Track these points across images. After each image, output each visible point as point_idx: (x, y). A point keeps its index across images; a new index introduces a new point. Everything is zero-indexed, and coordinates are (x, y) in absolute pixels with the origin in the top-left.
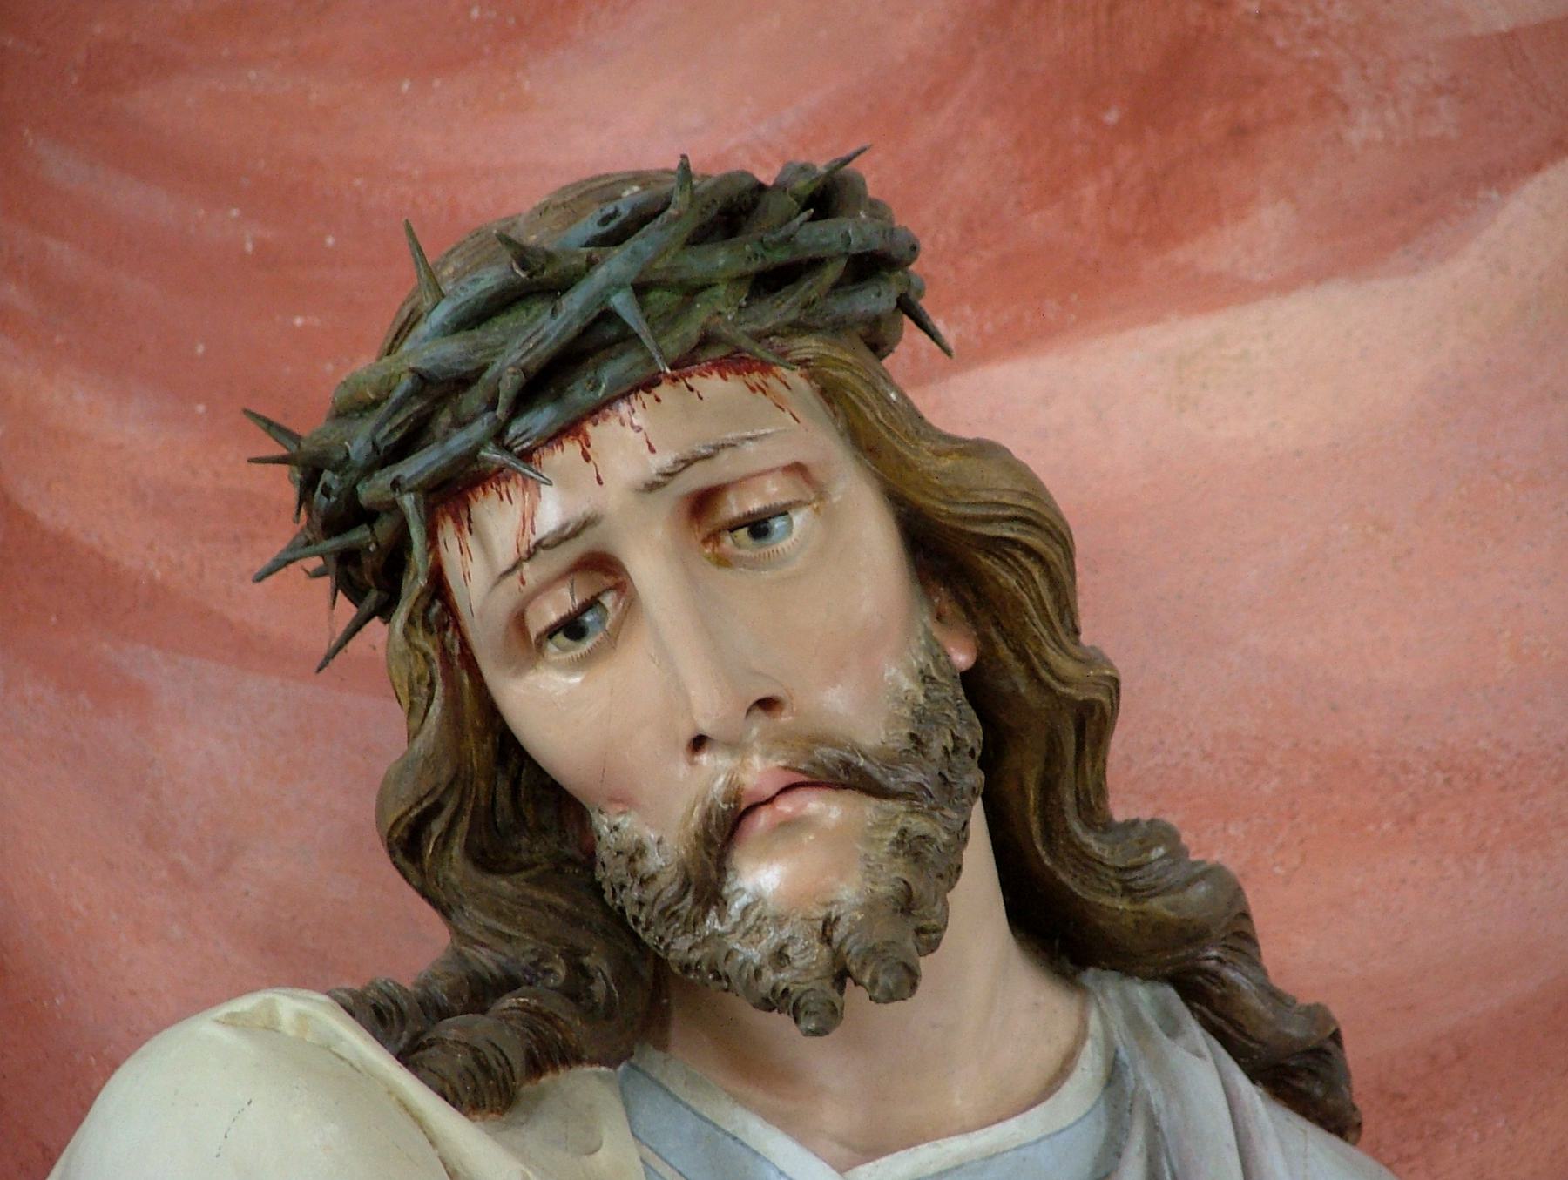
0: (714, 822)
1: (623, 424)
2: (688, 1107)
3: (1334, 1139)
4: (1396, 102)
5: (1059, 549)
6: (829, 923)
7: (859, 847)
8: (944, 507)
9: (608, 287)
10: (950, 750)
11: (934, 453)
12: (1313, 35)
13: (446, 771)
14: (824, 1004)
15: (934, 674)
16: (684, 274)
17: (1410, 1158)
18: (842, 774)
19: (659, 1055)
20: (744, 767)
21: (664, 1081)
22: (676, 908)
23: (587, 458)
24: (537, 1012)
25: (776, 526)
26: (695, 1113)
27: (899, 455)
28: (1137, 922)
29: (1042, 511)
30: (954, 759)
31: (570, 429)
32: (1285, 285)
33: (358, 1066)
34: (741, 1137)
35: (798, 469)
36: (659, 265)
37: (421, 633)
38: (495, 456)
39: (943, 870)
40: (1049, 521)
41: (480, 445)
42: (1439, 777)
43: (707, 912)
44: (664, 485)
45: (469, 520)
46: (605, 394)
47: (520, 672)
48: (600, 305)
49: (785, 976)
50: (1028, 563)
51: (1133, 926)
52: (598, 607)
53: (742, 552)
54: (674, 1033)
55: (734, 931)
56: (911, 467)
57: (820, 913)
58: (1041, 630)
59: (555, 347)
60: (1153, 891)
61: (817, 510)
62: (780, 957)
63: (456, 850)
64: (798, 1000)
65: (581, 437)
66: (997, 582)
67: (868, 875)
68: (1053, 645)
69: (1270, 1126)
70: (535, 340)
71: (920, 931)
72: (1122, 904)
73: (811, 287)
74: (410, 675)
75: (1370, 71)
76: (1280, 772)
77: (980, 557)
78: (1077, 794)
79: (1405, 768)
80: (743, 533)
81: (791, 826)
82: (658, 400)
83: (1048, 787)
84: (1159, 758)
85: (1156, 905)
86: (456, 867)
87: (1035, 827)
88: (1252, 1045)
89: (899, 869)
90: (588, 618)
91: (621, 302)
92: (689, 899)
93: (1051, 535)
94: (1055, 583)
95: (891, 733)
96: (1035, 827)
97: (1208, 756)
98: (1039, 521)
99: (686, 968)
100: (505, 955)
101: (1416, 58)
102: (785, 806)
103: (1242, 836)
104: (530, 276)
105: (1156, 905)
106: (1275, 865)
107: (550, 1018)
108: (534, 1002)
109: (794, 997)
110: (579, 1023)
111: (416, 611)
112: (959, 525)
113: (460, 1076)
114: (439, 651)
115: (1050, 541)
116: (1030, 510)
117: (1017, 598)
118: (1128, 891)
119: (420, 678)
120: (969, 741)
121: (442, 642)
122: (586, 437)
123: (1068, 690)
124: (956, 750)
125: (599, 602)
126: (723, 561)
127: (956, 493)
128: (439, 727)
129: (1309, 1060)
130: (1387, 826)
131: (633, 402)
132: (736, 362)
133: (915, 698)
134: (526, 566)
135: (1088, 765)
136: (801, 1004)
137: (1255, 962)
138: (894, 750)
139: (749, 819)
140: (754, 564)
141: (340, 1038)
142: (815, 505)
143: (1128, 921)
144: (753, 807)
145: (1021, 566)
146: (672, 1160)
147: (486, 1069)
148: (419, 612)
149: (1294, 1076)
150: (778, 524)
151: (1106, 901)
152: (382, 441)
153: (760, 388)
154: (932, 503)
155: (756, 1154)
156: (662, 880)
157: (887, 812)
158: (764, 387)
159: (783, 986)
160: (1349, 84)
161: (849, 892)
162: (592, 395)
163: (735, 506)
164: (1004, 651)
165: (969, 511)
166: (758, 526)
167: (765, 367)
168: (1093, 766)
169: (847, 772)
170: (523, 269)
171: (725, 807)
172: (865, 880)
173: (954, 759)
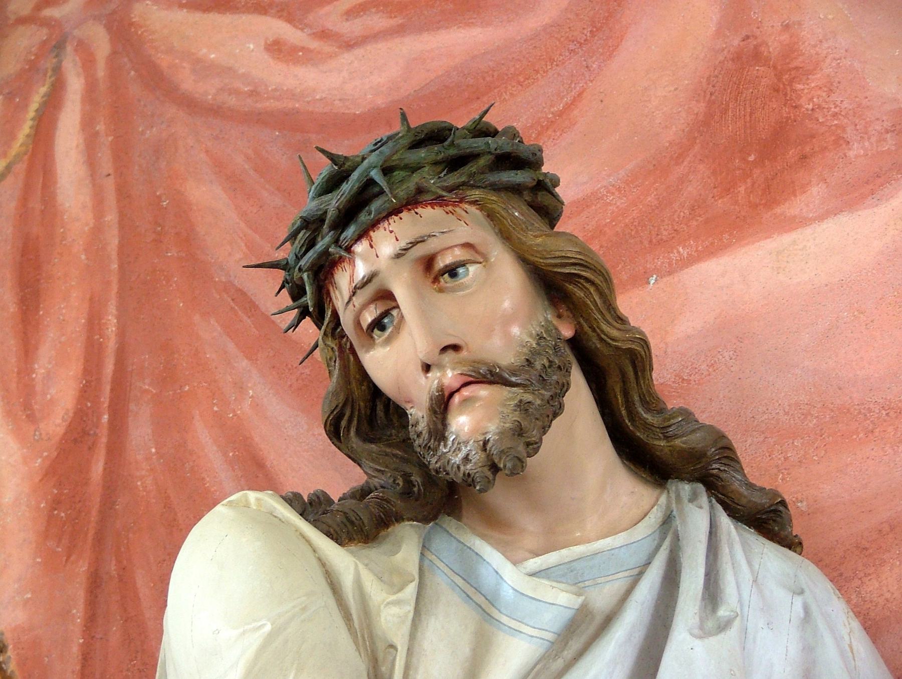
0: (434, 402)
1: (385, 230)
2: (455, 538)
3: (786, 551)
4: (869, 138)
5: (600, 278)
6: (486, 443)
7: (499, 408)
8: (542, 261)
9: (369, 168)
10: (547, 366)
11: (534, 236)
12: (835, 115)
13: (342, 398)
14: (483, 478)
15: (545, 336)
16: (406, 161)
17: (869, 574)
18: (489, 376)
19: (454, 521)
20: (444, 375)
21: (448, 529)
22: (428, 445)
23: (372, 247)
24: (382, 499)
25: (461, 271)
26: (458, 540)
27: (519, 238)
28: (670, 451)
29: (589, 260)
30: (549, 370)
31: (363, 234)
32: (821, 218)
33: (283, 520)
34: (472, 548)
35: (468, 246)
36: (395, 157)
37: (330, 339)
38: (345, 254)
39: (538, 416)
40: (593, 265)
41: (328, 247)
42: (884, 412)
43: (439, 445)
44: (404, 255)
45: (335, 284)
46: (374, 217)
47: (367, 351)
48: (366, 176)
49: (469, 467)
50: (587, 285)
51: (669, 453)
52: (390, 315)
53: (448, 285)
54: (464, 513)
55: (449, 451)
56: (524, 243)
57: (481, 438)
58: (598, 316)
59: (348, 197)
60: (676, 436)
61: (484, 266)
62: (466, 459)
63: (352, 433)
64: (474, 477)
65: (369, 238)
66: (576, 296)
67: (502, 420)
68: (605, 323)
69: (737, 539)
70: (340, 194)
71: (528, 444)
72: (662, 443)
73: (472, 167)
74: (326, 358)
75: (858, 127)
76: (817, 417)
77: (567, 285)
78: (640, 397)
79: (870, 410)
80: (446, 275)
81: (466, 401)
82: (401, 219)
83: (626, 394)
84: (766, 416)
85: (678, 442)
86: (355, 441)
87: (624, 412)
88: (739, 507)
89: (516, 416)
90: (386, 320)
91: (375, 174)
92: (432, 441)
93: (595, 271)
94: (601, 294)
95: (516, 358)
96: (624, 412)
97: (787, 413)
98: (588, 265)
99: (437, 472)
100: (383, 480)
101: (878, 119)
102: (466, 392)
103: (800, 445)
104: (339, 168)
105: (678, 442)
106: (814, 456)
107: (388, 501)
108: (381, 494)
109: (472, 476)
110: (399, 502)
111: (328, 330)
112: (550, 269)
113: (338, 525)
114: (338, 346)
115: (595, 274)
116: (581, 259)
117: (584, 302)
118: (667, 438)
119: (331, 359)
120: (557, 362)
121: (340, 342)
122: (371, 237)
123: (616, 344)
124: (550, 367)
125: (390, 313)
126: (441, 290)
127: (545, 253)
128: (338, 378)
129: (772, 515)
130: (861, 435)
131: (390, 220)
132: (439, 201)
133: (531, 345)
134: (354, 298)
135: (642, 382)
136: (474, 479)
137: (741, 470)
138: (517, 366)
139: (451, 401)
140: (453, 290)
141: (275, 508)
142: (484, 264)
143: (666, 450)
144: (451, 395)
145: (586, 288)
146: (444, 560)
147: (352, 523)
148: (330, 331)
149: (766, 523)
150: (461, 270)
151: (656, 442)
152: (299, 253)
153: (451, 212)
154: (536, 259)
155: (477, 554)
156: (424, 432)
157: (514, 393)
158: (453, 211)
159: (467, 472)
160: (850, 133)
161: (492, 428)
162: (368, 217)
163: (442, 262)
164: (586, 328)
165: (553, 261)
166: (452, 271)
167: (454, 204)
168: (644, 383)
169: (492, 376)
170: (336, 165)
171: (437, 394)
172: (500, 422)
173: (549, 370)
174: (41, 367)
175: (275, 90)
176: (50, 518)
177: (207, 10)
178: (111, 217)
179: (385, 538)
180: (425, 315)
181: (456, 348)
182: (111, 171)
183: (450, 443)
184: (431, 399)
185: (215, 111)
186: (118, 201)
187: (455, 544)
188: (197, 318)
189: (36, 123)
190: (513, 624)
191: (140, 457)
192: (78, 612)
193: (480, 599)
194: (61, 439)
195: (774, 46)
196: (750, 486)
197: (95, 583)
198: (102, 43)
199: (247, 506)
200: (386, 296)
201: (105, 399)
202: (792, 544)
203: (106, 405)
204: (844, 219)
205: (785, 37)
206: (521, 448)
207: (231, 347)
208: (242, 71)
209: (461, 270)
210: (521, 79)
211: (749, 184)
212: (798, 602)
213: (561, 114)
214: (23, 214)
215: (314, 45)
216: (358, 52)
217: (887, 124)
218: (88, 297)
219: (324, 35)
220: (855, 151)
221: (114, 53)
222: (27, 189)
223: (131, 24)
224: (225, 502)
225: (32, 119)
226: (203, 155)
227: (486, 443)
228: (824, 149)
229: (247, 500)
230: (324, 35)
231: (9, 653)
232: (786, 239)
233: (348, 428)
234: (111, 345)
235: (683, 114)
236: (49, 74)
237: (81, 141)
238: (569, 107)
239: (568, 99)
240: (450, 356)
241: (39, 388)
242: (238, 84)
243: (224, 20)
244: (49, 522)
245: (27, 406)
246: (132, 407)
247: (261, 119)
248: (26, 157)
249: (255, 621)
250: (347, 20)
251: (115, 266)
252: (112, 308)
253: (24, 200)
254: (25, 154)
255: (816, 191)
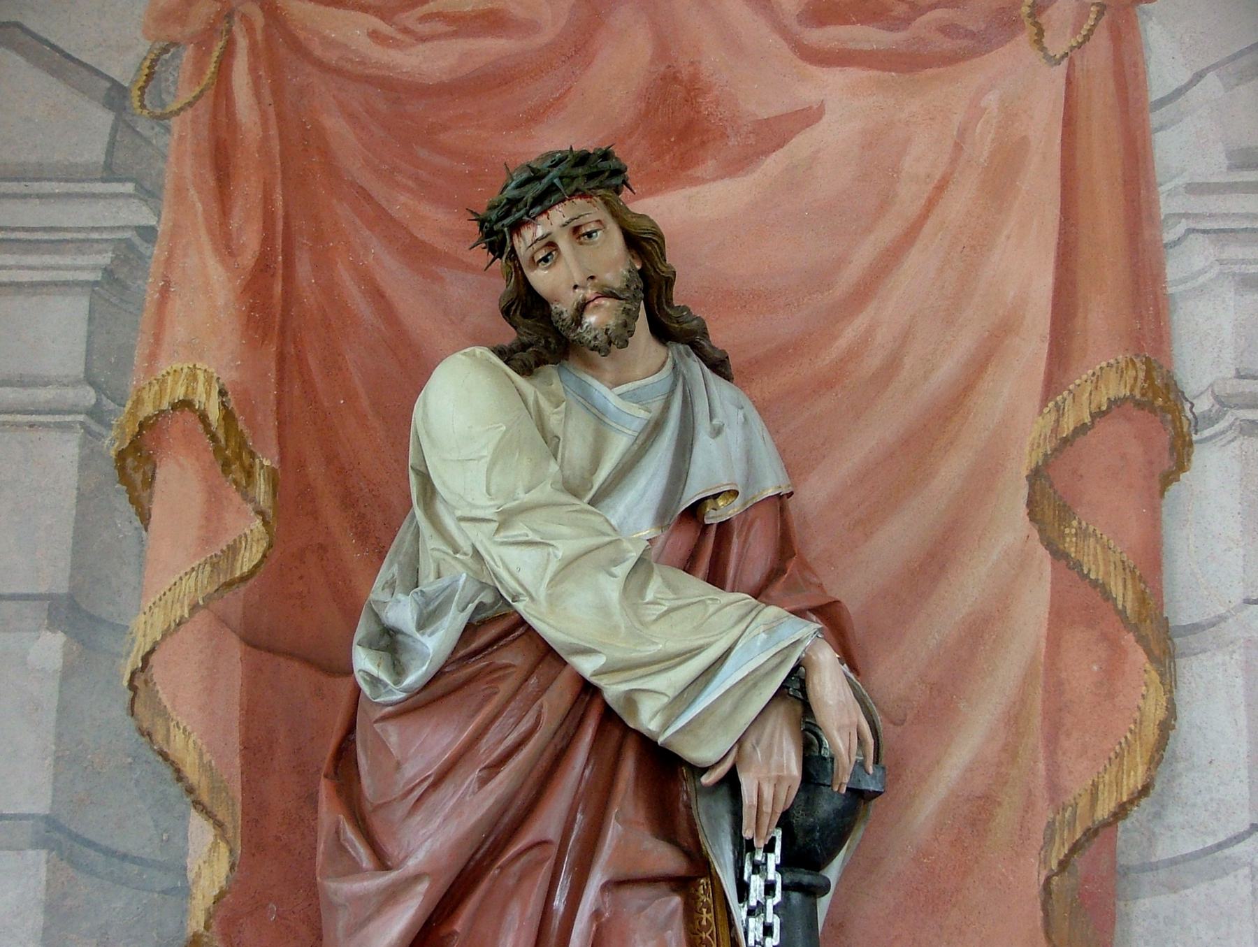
6: (607, 330)
12: (720, 119)
19: (565, 361)
31: (544, 212)
32: (714, 180)
35: (598, 221)
41: (523, 216)
47: (533, 271)
62: (595, 338)
79: (743, 294)
81: (596, 306)
85: (684, 326)
86: (518, 318)
87: (656, 307)
91: (556, 181)
94: (660, 248)
102: (596, 302)
105: (684, 326)
118: (678, 322)
126: (581, 244)
132: (584, 196)
144: (589, 302)
160: (729, 130)
161: (612, 322)
163: (583, 230)
166: (589, 235)
167: (591, 197)
174: (234, 224)
175: (377, 62)
176: (249, 318)
177: (328, 5)
178: (273, 132)
179: (538, 373)
180: (579, 261)
181: (592, 278)
182: (272, 102)
183: (585, 326)
184: (578, 304)
185: (338, 71)
186: (278, 122)
187: (574, 378)
188: (335, 201)
189: (218, 65)
190: (619, 427)
191: (304, 284)
192: (272, 376)
193: (595, 411)
194: (252, 269)
195: (685, 74)
196: (713, 347)
197: (281, 359)
198: (259, 20)
199: (474, 355)
200: (552, 245)
201: (279, 246)
202: (728, 378)
203: (280, 250)
204: (727, 181)
205: (691, 69)
206: (626, 334)
207: (358, 221)
208: (354, 48)
209: (594, 234)
210: (533, 75)
211: (672, 154)
212: (741, 413)
213: (558, 99)
214: (214, 126)
215: (400, 36)
216: (429, 45)
217: (750, 128)
218: (262, 181)
219: (406, 31)
220: (732, 142)
221: (267, 26)
222: (216, 107)
223: (277, 8)
224: (462, 352)
225: (215, 62)
226: (331, 99)
227: (607, 330)
228: (715, 139)
229: (475, 352)
230: (406, 31)
231: (229, 397)
232: (694, 190)
233: (515, 311)
234: (280, 212)
235: (632, 108)
236: (224, 33)
237: (250, 81)
238: (561, 96)
239: (562, 91)
240: (590, 283)
241: (234, 236)
242: (351, 56)
243: (341, 13)
244: (248, 321)
245: (228, 247)
246: (297, 253)
247: (368, 80)
248: (213, 87)
249: (495, 423)
250: (420, 23)
251: (278, 163)
252: (279, 190)
253: (215, 116)
254: (213, 84)
255: (711, 163)
